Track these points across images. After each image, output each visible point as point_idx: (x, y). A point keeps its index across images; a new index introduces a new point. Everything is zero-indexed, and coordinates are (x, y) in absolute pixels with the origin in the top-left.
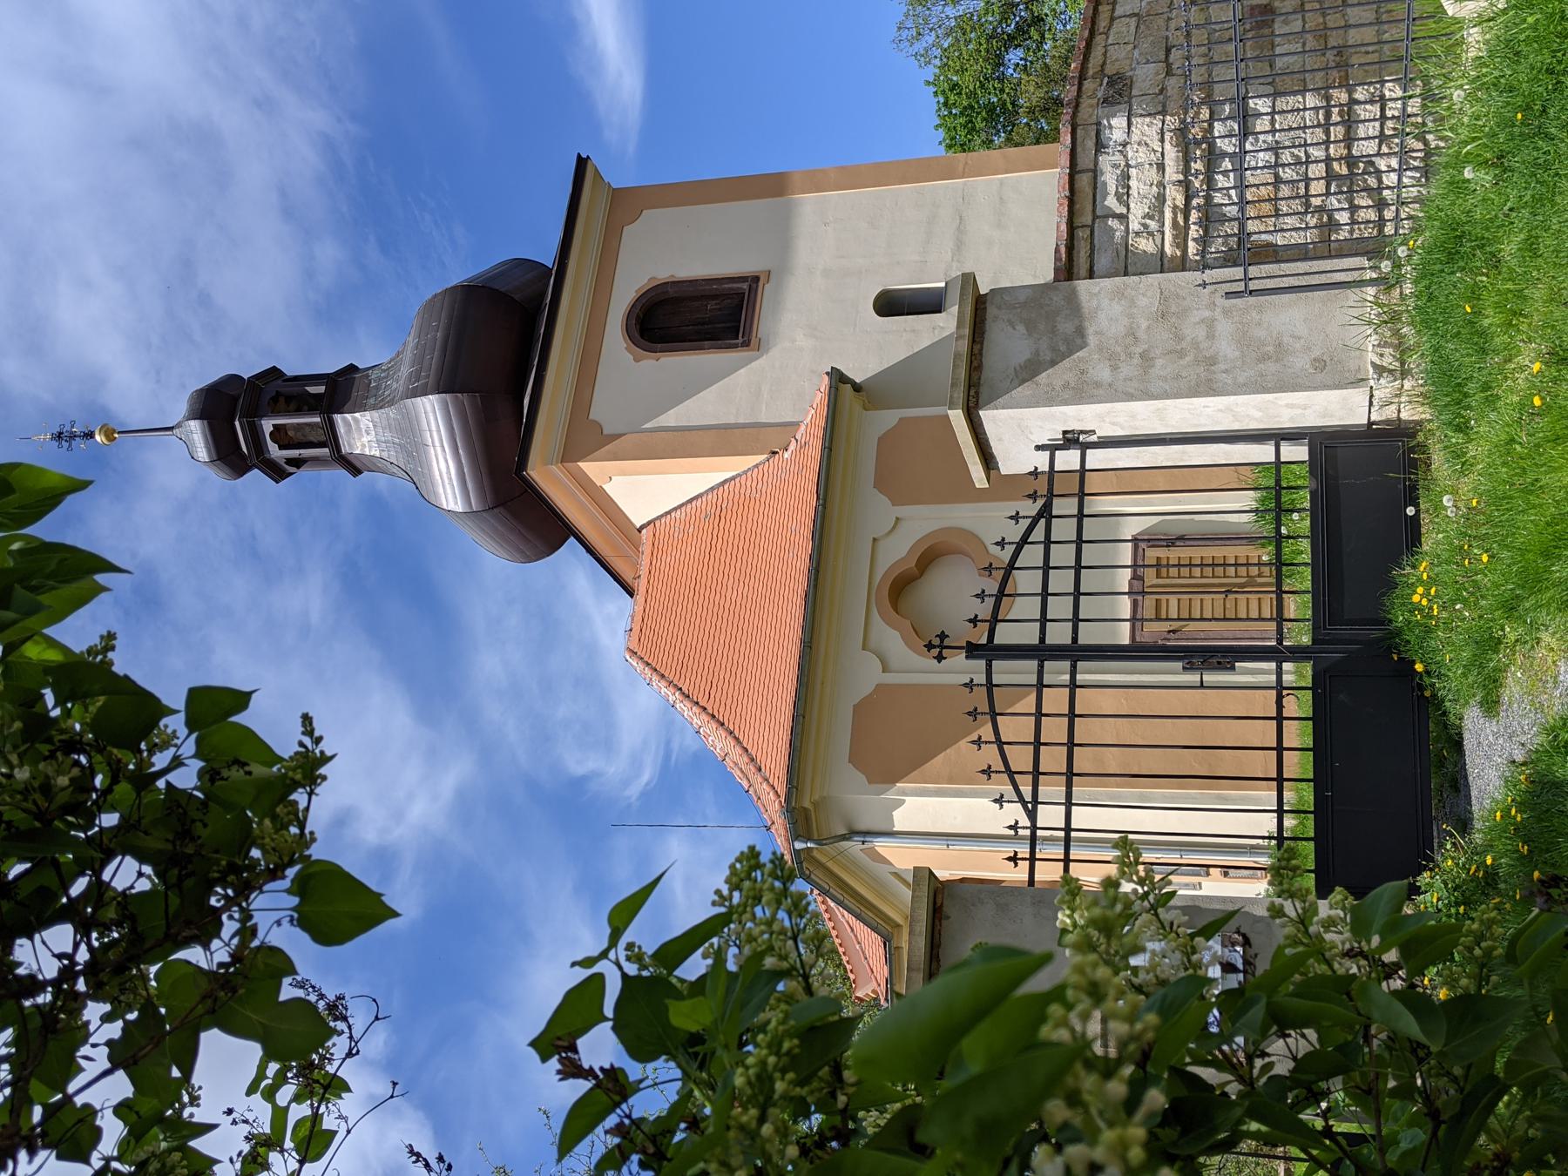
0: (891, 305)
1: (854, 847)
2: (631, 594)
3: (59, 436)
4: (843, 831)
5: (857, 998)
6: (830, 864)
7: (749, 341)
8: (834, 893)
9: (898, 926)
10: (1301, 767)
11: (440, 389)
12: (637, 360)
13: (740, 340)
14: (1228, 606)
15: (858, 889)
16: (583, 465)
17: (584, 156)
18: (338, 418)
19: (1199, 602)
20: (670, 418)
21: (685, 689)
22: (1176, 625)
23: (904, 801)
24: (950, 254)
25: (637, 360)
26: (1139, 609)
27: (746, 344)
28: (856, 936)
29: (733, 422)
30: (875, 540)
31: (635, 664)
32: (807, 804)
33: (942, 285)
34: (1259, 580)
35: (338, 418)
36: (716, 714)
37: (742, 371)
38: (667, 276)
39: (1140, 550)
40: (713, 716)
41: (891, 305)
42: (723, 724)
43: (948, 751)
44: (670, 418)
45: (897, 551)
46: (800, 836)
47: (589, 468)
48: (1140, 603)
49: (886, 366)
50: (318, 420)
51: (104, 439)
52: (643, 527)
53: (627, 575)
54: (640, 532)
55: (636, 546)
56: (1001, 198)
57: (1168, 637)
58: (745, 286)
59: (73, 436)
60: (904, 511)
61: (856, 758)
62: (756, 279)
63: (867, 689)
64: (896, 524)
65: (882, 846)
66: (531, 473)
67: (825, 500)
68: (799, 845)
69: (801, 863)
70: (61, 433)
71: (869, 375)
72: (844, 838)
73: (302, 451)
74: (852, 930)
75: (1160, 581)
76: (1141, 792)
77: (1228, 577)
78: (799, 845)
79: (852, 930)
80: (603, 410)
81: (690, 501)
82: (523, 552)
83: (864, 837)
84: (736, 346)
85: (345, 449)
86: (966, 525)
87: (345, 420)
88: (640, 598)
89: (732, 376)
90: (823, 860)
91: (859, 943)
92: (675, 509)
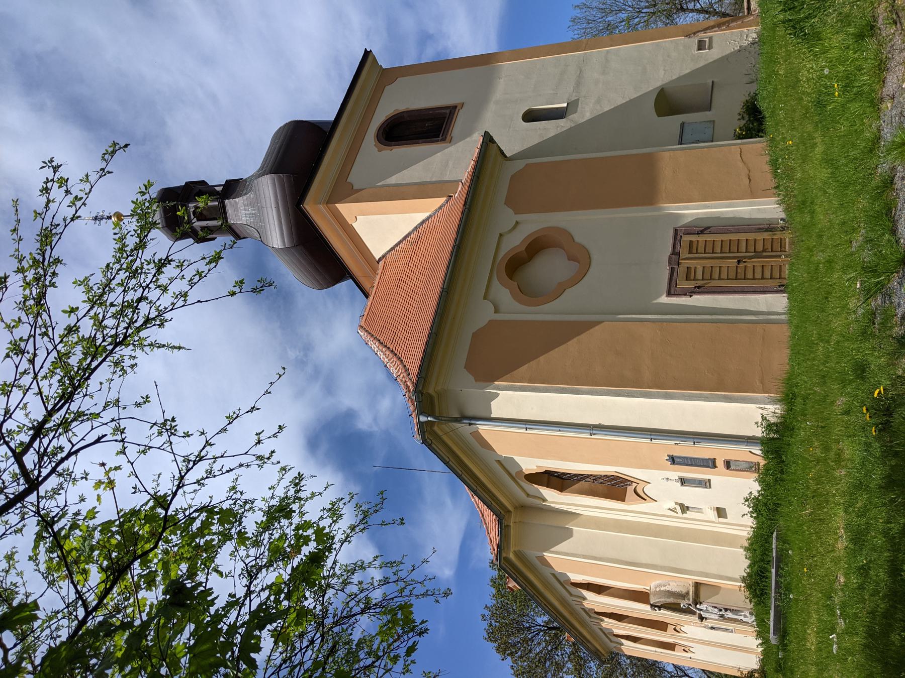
0: (531, 116)
1: (464, 428)
2: (367, 296)
3: (96, 218)
4: (457, 415)
5: (509, 587)
6: (445, 438)
7: (446, 138)
8: (464, 477)
9: (509, 512)
10: (792, 350)
11: (271, 172)
12: (379, 151)
13: (441, 138)
14: (739, 271)
15: (472, 468)
16: (340, 206)
17: (368, 50)
18: (226, 201)
19: (718, 269)
20: (393, 180)
21: (382, 341)
22: (700, 283)
23: (498, 395)
24: (572, 89)
25: (379, 151)
26: (675, 274)
27: (444, 140)
28: (484, 519)
29: (428, 180)
30: (501, 235)
31: (362, 334)
32: (431, 391)
33: (565, 105)
34: (765, 254)
35: (226, 201)
36: (394, 350)
37: (439, 154)
38: (404, 108)
39: (679, 237)
40: (392, 351)
41: (531, 116)
42: (396, 355)
43: (531, 363)
44: (393, 180)
45: (515, 242)
46: (424, 412)
47: (342, 207)
48: (676, 270)
49: (525, 148)
50: (217, 203)
51: (116, 220)
52: (380, 259)
53: (366, 285)
54: (378, 263)
55: (375, 271)
56: (607, 60)
57: (694, 291)
58: (448, 111)
59: (102, 219)
60: (520, 217)
61: (468, 367)
62: (455, 107)
63: (482, 323)
64: (514, 228)
65: (484, 428)
66: (306, 207)
67: (470, 206)
68: (423, 419)
69: (424, 432)
70: (96, 217)
71: (514, 153)
72: (457, 420)
73: (208, 222)
74: (483, 516)
75: (691, 256)
76: (666, 392)
77: (741, 252)
78: (423, 419)
79: (483, 516)
80: (356, 177)
81: (404, 238)
82: (318, 281)
83: (470, 420)
84: (437, 141)
85: (231, 221)
86: (562, 225)
87: (230, 202)
88: (371, 298)
89: (432, 157)
90: (440, 433)
91: (486, 524)
92: (396, 245)
